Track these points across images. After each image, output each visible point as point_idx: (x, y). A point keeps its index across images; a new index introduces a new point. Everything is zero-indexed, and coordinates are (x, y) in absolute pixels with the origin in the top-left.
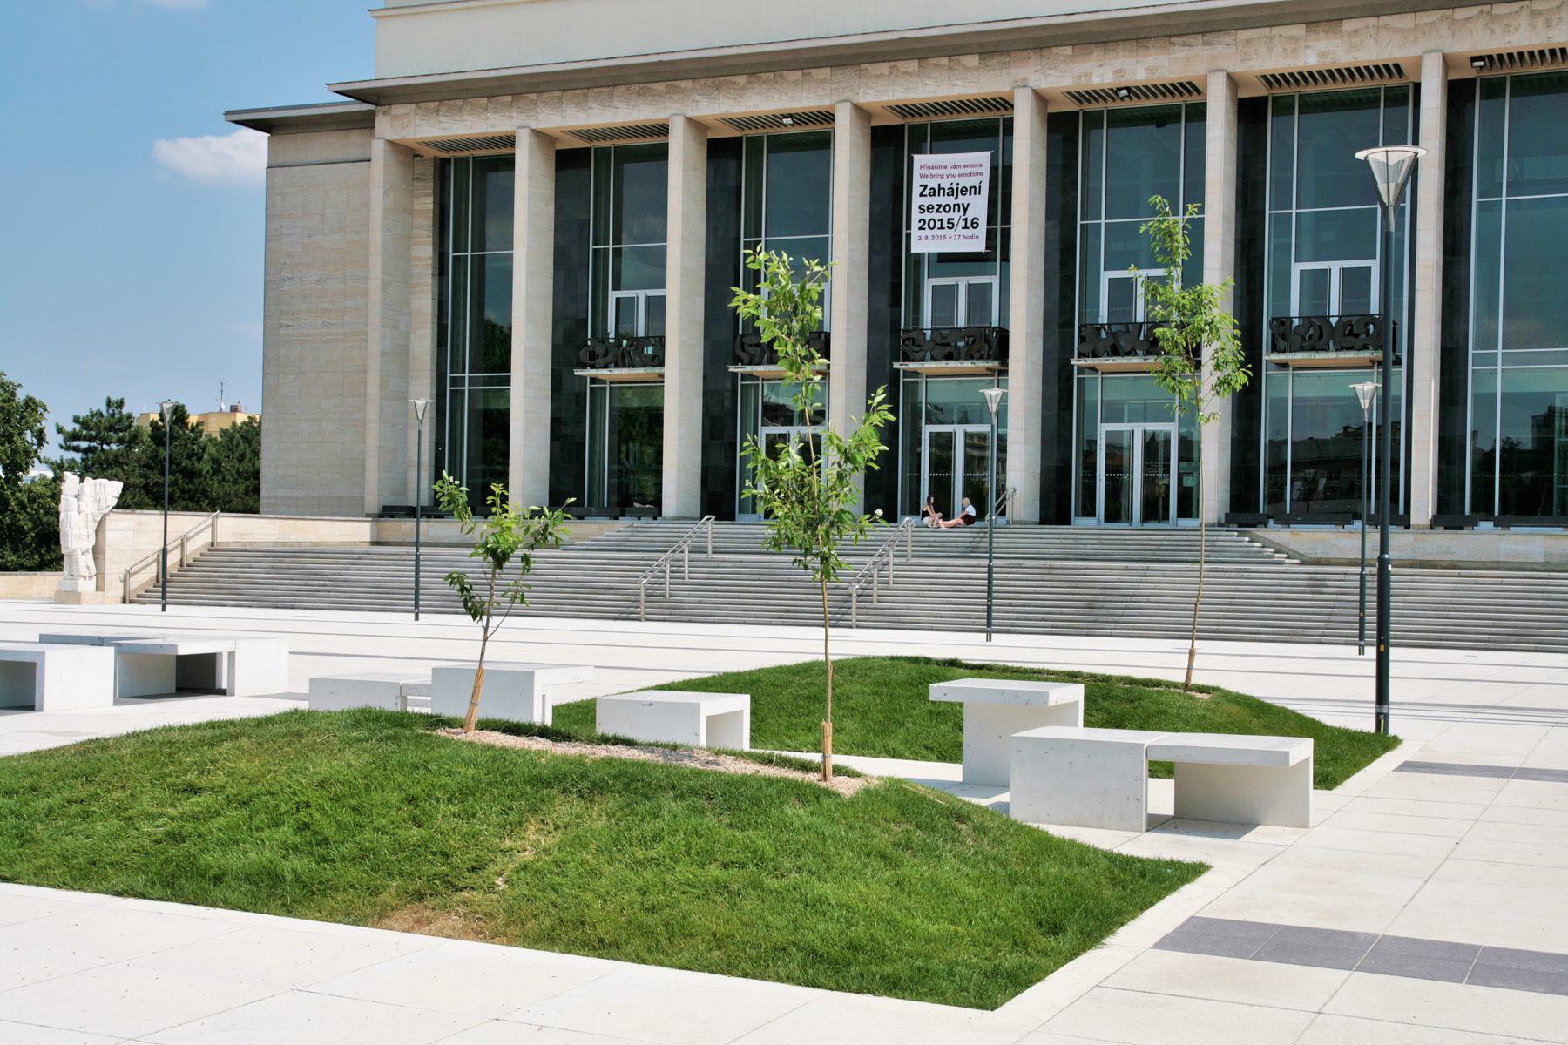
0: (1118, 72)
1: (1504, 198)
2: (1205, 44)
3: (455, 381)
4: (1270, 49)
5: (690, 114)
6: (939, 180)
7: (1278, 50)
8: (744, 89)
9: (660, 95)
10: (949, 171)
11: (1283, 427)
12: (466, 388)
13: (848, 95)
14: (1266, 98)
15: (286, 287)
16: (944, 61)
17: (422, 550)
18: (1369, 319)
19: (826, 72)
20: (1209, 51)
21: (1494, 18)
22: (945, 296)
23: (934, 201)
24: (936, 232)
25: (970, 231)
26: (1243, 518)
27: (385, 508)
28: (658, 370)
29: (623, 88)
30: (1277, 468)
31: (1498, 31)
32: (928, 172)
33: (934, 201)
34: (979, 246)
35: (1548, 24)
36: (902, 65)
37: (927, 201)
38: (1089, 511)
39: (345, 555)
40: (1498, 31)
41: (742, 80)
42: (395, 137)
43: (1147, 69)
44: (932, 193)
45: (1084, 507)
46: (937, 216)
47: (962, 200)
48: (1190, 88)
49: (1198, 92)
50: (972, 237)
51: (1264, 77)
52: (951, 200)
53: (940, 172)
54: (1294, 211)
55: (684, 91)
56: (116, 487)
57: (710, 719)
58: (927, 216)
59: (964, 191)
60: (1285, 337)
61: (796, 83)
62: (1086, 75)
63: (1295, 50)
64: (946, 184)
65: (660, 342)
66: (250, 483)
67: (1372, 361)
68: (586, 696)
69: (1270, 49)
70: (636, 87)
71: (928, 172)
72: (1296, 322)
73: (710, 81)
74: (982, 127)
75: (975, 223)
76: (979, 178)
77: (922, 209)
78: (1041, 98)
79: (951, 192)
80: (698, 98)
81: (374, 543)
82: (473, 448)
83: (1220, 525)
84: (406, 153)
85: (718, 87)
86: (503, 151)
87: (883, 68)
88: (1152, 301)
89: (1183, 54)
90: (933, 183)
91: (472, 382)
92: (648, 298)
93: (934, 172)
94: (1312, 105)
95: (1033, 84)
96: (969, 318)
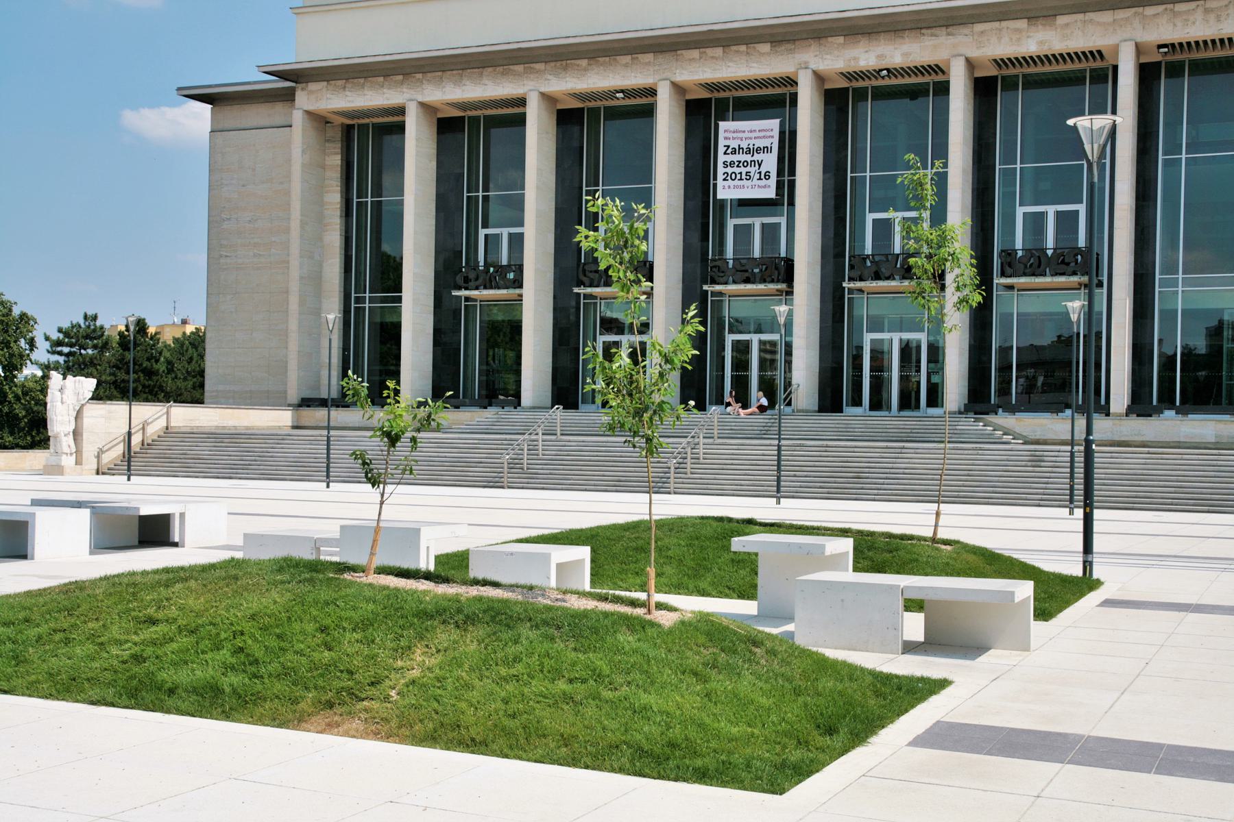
0: (880, 57)
1: (1184, 156)
2: (948, 34)
3: (358, 300)
4: (1000, 39)
5: (543, 90)
6: (739, 142)
7: (1006, 39)
8: (586, 70)
9: (519, 75)
10: (747, 135)
11: (1009, 336)
12: (367, 305)
13: (668, 74)
14: (996, 77)
15: (225, 225)
16: (743, 48)
17: (332, 433)
18: (1078, 251)
19: (650, 57)
20: (951, 40)
21: (1176, 14)
22: (743, 233)
23: (735, 158)
24: (737, 182)
25: (764, 182)
26: (978, 407)
27: (303, 400)
28: (518, 291)
29: (490, 69)
30: (1005, 369)
31: (1179, 24)
32: (730, 135)
33: (735, 158)
34: (770, 193)
35: (1218, 19)
36: (710, 51)
37: (729, 158)
38: (857, 402)
39: (272, 437)
40: (1179, 24)
41: (584, 63)
42: (311, 108)
43: (903, 55)
44: (734, 152)
45: (853, 398)
46: (737, 170)
47: (757, 157)
48: (936, 69)
49: (943, 72)
50: (765, 187)
51: (995, 61)
52: (748, 158)
53: (740, 135)
54: (1018, 166)
55: (538, 72)
56: (91, 383)
57: (559, 566)
58: (729, 170)
59: (758, 150)
60: (1011, 265)
61: (626, 65)
62: (855, 59)
63: (1019, 39)
64: (744, 145)
65: (520, 269)
66: (197, 380)
67: (1080, 284)
68: (461, 548)
69: (1000, 39)
70: (501, 69)
71: (730, 135)
72: (1020, 253)
73: (559, 64)
74: (773, 100)
75: (767, 176)
76: (771, 140)
77: (725, 164)
78: (819, 77)
79: (749, 151)
80: (549, 77)
81: (294, 427)
82: (372, 353)
83: (960, 413)
84: (320, 121)
85: (565, 69)
86: (396, 119)
87: (695, 53)
88: (906, 237)
89: (931, 43)
90: (734, 144)
91: (372, 300)
92: (510, 235)
93: (735, 135)
94: (1033, 83)
95: (813, 66)
96: (762, 250)
